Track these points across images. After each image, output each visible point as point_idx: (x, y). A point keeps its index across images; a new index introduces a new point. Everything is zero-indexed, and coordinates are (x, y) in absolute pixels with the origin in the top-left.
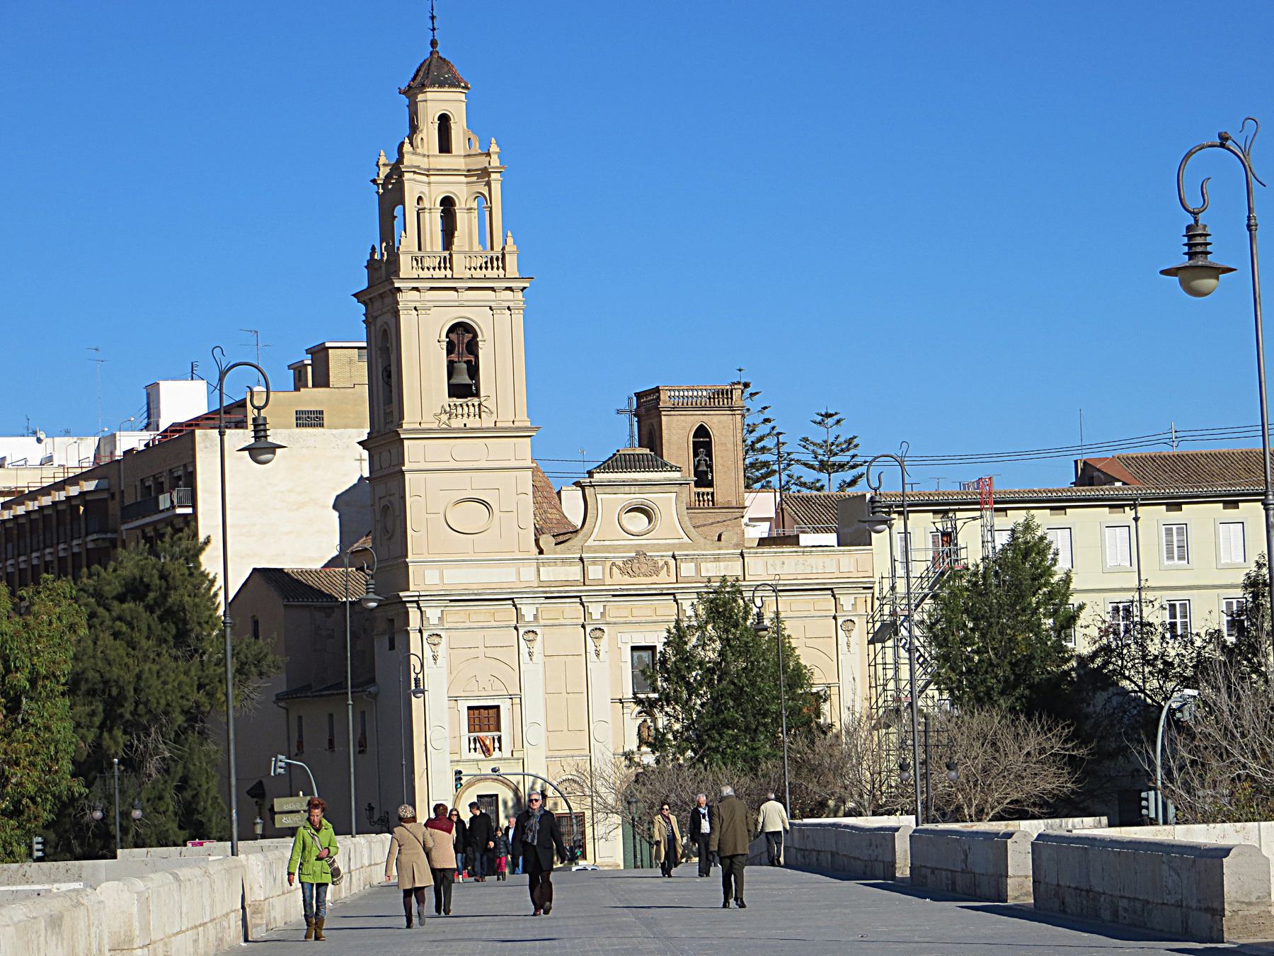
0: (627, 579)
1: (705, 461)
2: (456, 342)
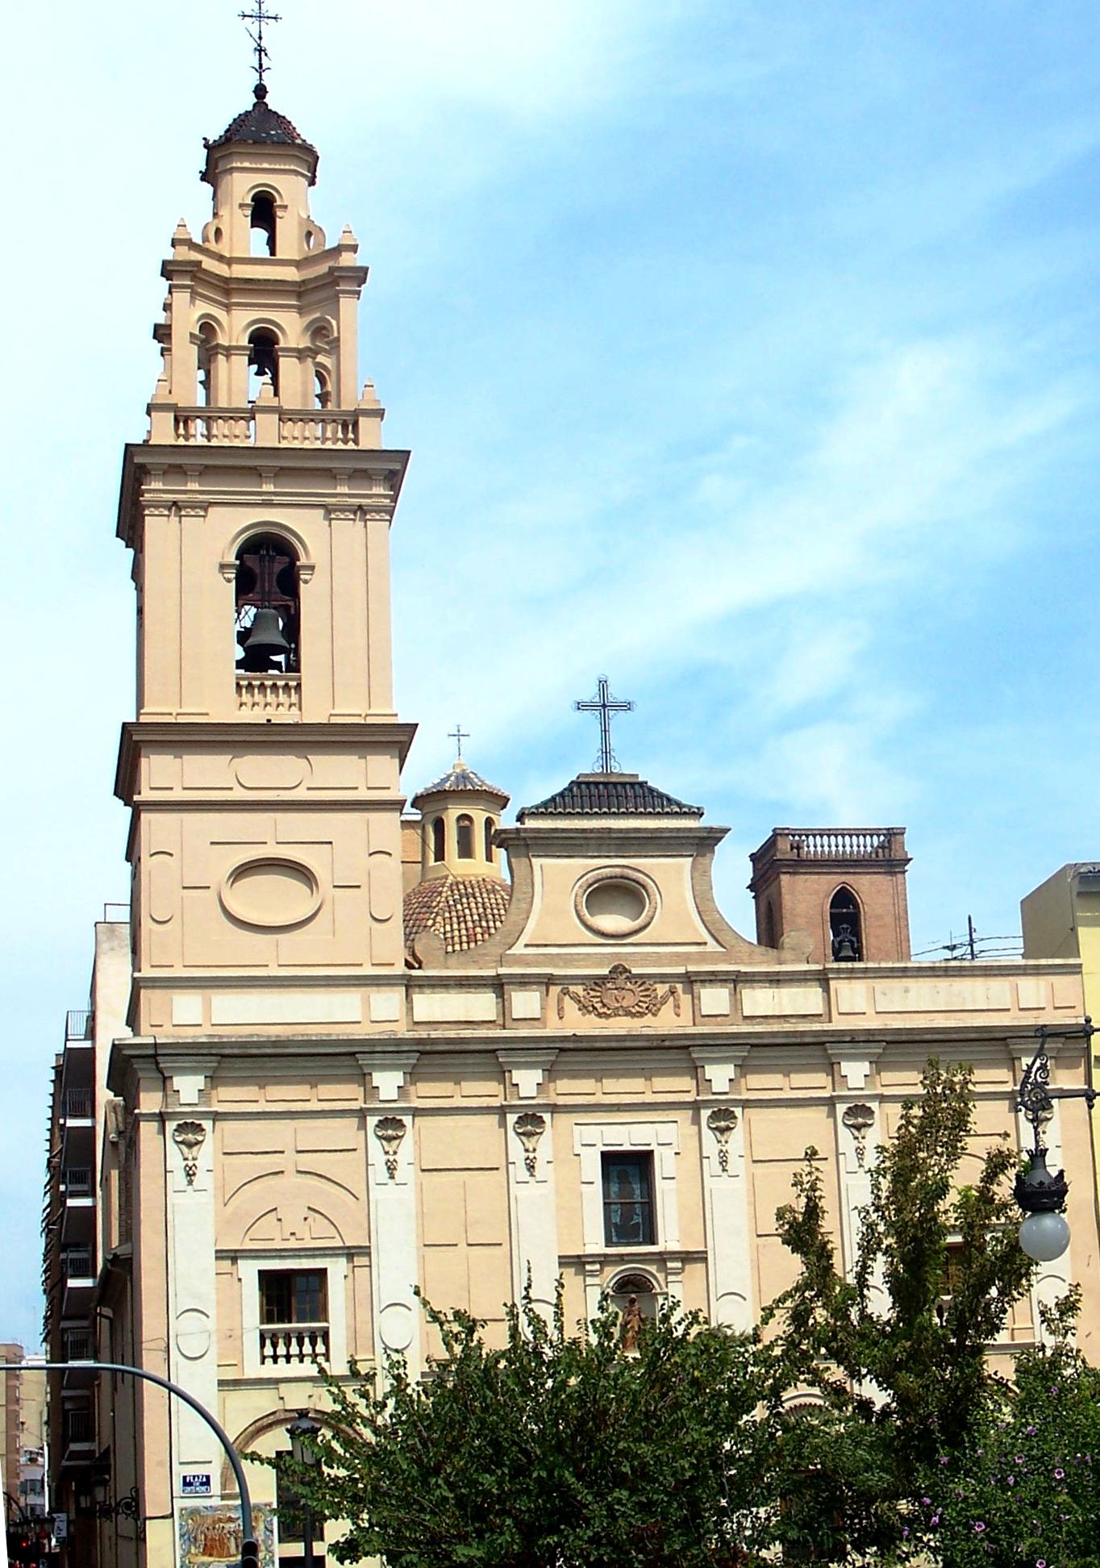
2: (258, 571)
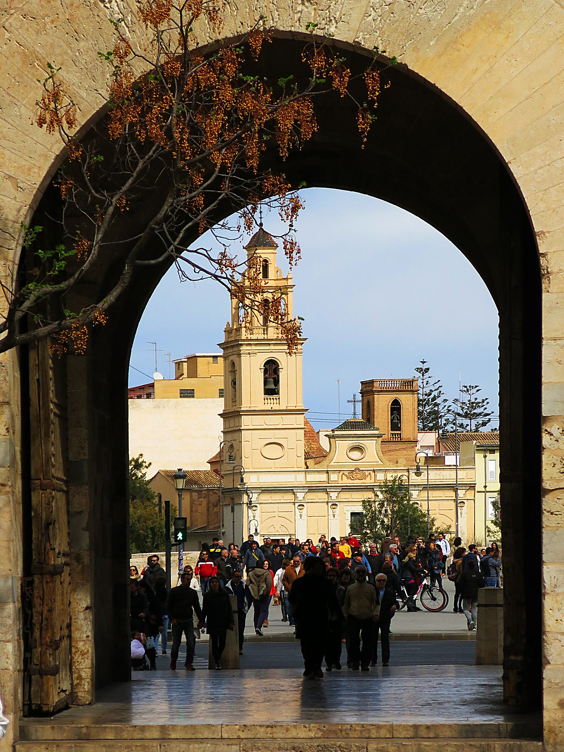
0: (350, 481)
1: (397, 417)
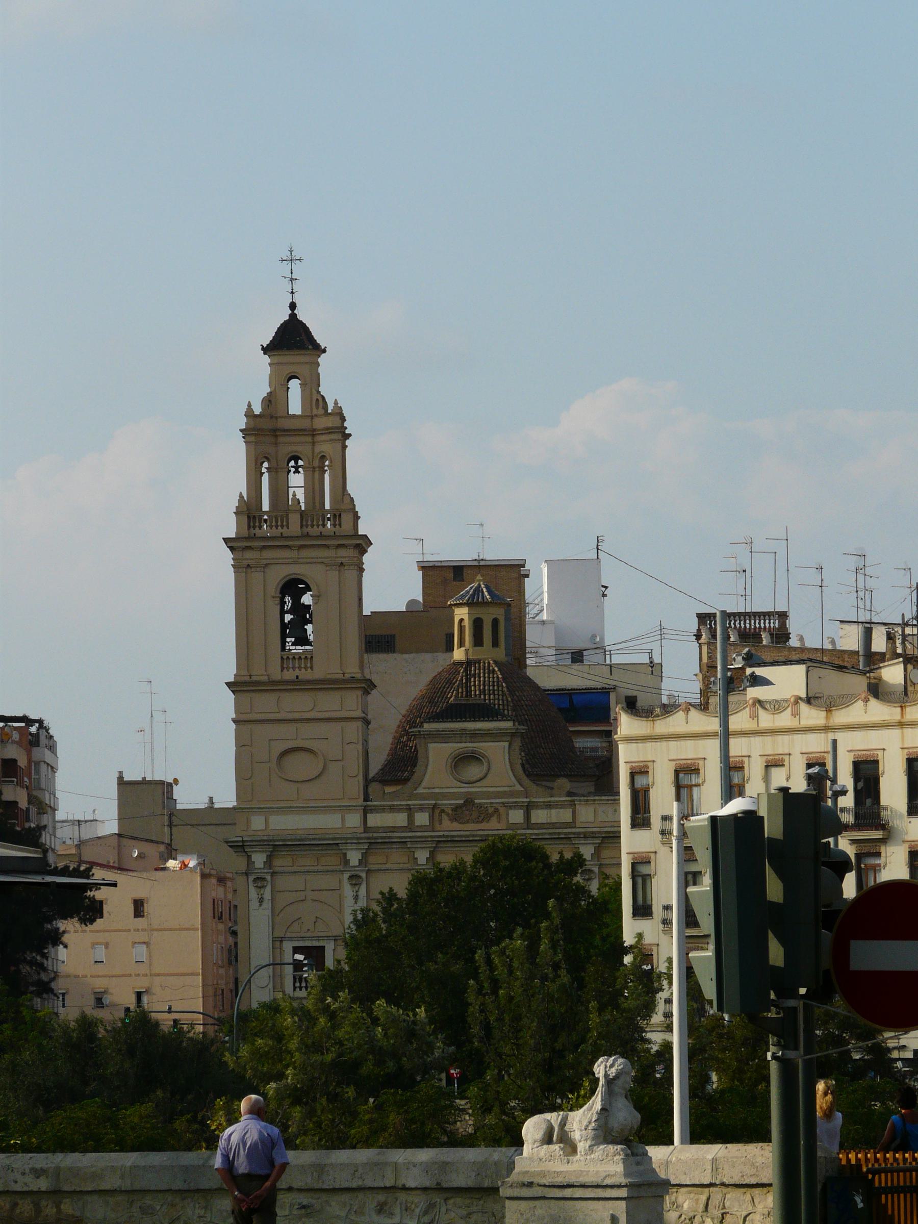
0: (456, 825)
